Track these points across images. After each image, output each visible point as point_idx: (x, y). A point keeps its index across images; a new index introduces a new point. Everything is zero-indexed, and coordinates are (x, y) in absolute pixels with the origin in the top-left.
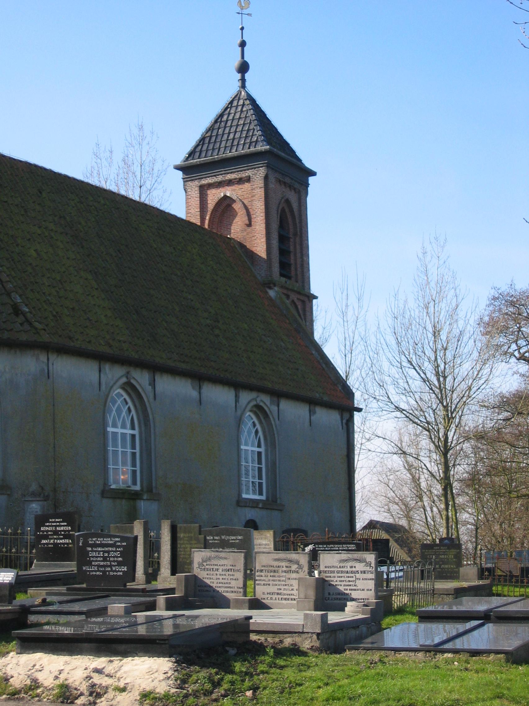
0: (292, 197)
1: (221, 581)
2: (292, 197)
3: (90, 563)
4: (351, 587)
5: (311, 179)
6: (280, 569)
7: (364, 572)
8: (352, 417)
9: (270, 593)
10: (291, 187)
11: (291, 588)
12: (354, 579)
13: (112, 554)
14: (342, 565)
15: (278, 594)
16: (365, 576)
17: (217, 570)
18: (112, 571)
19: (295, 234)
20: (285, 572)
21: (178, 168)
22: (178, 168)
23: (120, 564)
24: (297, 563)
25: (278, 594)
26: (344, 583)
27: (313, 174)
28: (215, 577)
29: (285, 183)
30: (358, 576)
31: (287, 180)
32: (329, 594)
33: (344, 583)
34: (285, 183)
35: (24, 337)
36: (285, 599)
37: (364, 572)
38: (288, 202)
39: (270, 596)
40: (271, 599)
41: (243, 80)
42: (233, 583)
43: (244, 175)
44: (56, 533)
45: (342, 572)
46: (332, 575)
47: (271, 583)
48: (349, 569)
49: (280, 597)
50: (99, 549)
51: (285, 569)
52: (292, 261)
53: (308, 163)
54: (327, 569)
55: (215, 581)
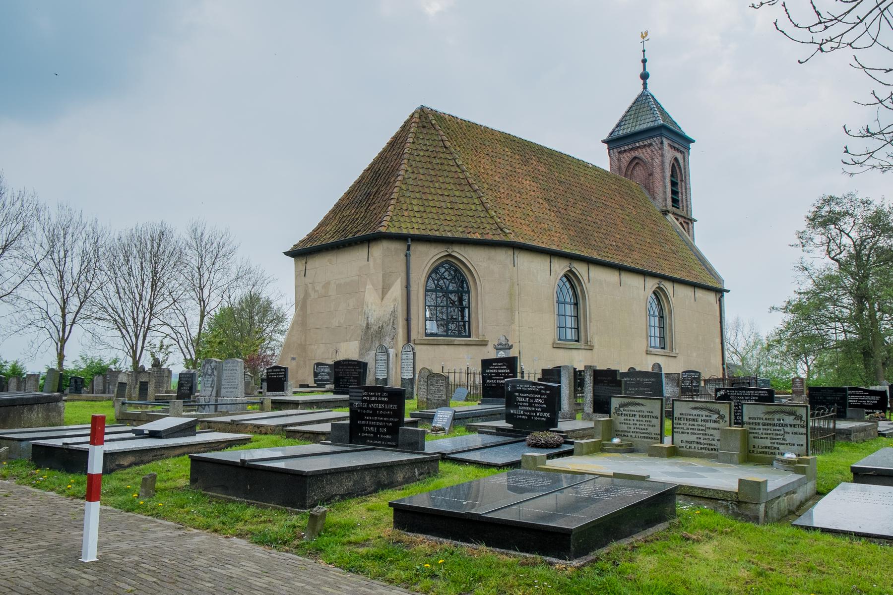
0: (679, 156)
1: (638, 426)
2: (679, 156)
3: (517, 407)
4: (779, 441)
5: (691, 145)
6: (700, 418)
7: (794, 426)
8: (722, 296)
9: (689, 442)
10: (678, 150)
11: (711, 438)
12: (782, 432)
13: (536, 401)
14: (767, 416)
15: (697, 443)
16: (796, 430)
17: (635, 415)
18: (536, 416)
19: (682, 181)
20: (705, 421)
21: (604, 142)
22: (604, 142)
23: (544, 410)
24: (718, 412)
25: (697, 443)
26: (771, 436)
27: (693, 141)
28: (632, 422)
29: (674, 148)
30: (787, 429)
31: (677, 146)
32: (754, 447)
33: (771, 436)
34: (674, 148)
35: (496, 238)
36: (705, 449)
37: (794, 426)
38: (676, 159)
39: (688, 445)
40: (690, 447)
41: (645, 85)
42: (651, 430)
43: (646, 143)
44: (498, 374)
45: (768, 424)
46: (757, 427)
47: (690, 431)
48: (776, 422)
49: (700, 446)
50: (526, 395)
51: (704, 418)
52: (680, 198)
53: (688, 134)
54: (751, 421)
55: (633, 427)
